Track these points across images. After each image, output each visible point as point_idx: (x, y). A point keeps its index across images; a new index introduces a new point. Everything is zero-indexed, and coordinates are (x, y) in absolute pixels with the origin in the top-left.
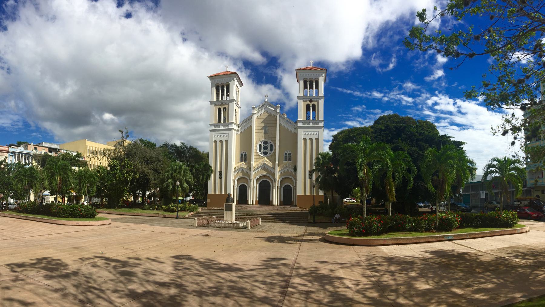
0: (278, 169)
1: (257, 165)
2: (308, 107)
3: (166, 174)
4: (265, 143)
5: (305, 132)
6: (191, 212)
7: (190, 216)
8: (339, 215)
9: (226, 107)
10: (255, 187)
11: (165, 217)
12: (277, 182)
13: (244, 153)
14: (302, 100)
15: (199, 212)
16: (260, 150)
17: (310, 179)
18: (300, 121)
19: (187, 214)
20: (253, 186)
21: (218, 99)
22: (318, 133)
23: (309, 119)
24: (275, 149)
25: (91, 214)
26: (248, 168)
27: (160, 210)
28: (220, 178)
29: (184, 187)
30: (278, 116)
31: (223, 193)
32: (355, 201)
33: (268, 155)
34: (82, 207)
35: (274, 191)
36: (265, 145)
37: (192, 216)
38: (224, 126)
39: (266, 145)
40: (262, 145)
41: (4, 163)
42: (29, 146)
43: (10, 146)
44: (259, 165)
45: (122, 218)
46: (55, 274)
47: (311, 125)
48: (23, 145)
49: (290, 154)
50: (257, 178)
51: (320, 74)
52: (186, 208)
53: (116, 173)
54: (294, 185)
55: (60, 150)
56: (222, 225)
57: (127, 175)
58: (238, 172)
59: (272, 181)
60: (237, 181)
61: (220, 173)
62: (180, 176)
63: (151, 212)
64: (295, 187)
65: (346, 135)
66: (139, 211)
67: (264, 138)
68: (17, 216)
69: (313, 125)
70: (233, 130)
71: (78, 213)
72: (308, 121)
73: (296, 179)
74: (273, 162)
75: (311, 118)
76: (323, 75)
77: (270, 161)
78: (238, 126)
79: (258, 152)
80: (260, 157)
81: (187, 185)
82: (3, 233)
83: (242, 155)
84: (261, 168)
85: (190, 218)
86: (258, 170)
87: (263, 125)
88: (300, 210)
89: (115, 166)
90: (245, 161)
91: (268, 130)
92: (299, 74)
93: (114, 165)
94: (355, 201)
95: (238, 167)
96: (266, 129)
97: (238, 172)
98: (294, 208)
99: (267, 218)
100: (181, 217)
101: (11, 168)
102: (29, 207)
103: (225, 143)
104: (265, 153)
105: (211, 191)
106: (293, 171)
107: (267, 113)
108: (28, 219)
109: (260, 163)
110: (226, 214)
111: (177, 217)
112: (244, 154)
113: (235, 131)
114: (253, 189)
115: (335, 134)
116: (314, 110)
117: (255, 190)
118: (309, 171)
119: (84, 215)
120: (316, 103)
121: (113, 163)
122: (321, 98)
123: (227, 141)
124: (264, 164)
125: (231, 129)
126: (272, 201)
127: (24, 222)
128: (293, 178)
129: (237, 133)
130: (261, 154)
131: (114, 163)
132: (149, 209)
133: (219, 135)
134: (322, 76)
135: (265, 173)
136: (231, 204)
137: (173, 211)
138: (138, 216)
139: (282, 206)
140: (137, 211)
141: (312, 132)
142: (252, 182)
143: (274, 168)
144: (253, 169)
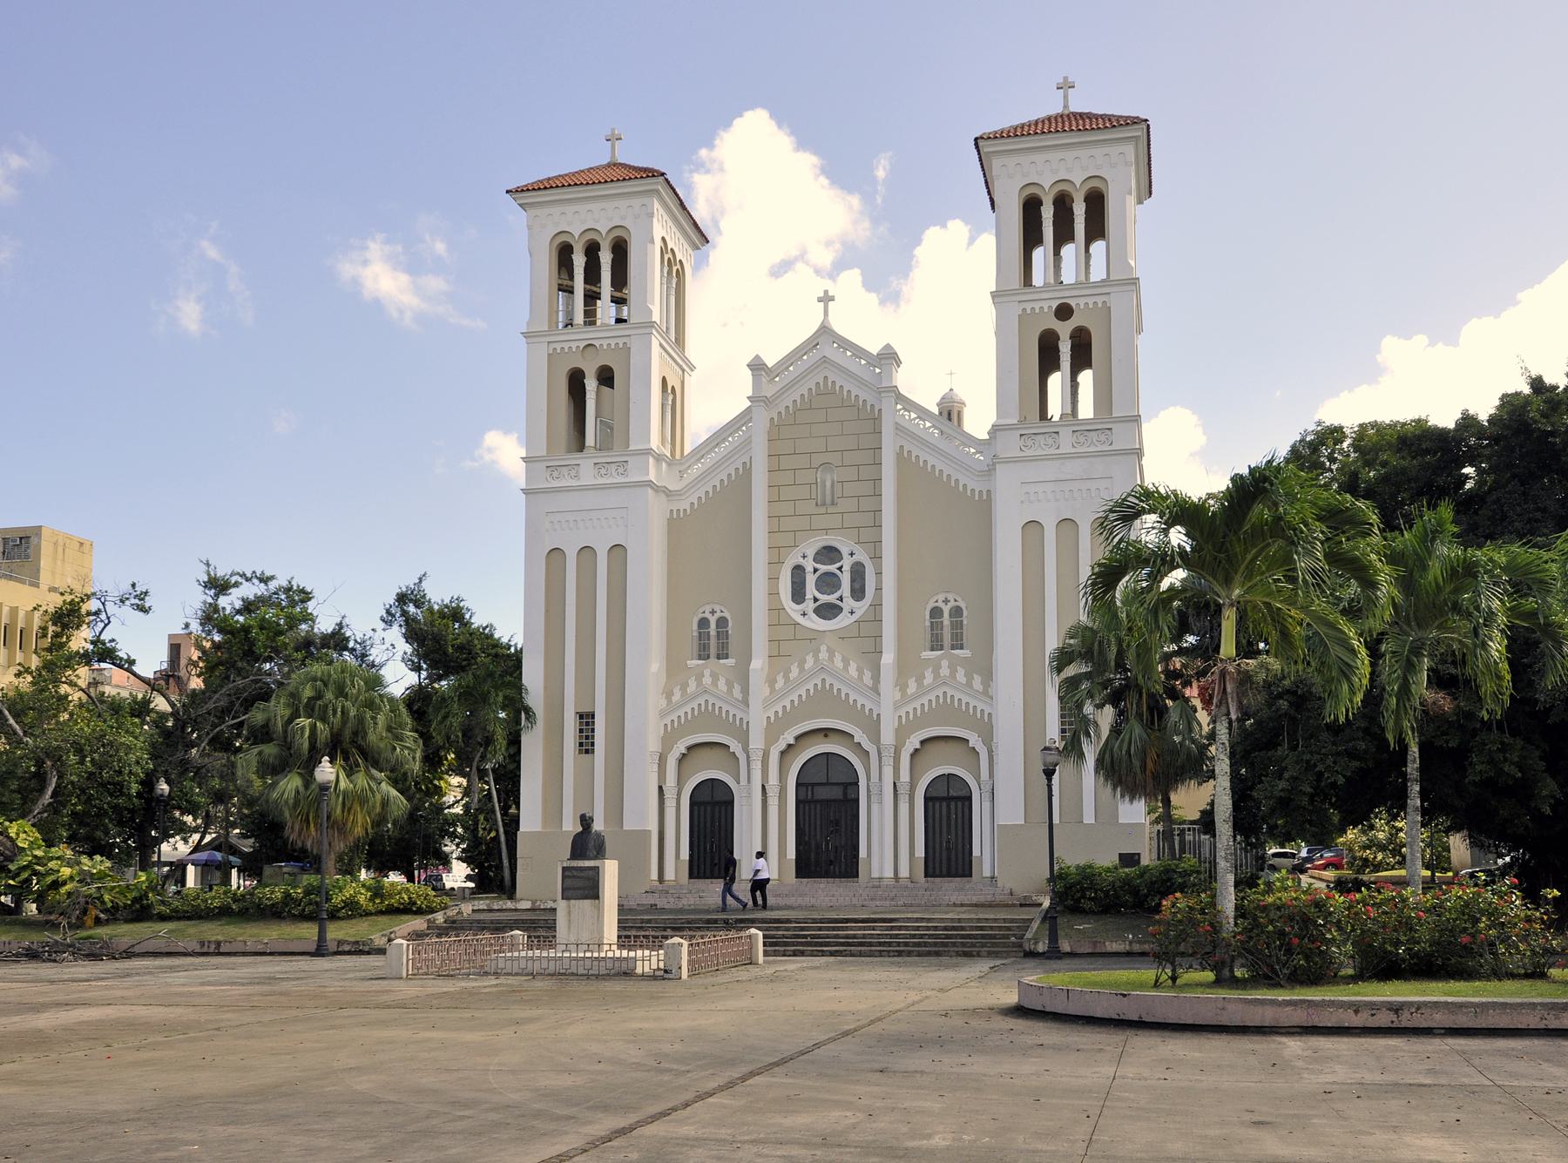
36: (823, 568)
39: (832, 568)
40: (809, 569)
91: (838, 487)
92: (984, 150)
111: (320, 951)
112: (946, 610)
128: (974, 740)
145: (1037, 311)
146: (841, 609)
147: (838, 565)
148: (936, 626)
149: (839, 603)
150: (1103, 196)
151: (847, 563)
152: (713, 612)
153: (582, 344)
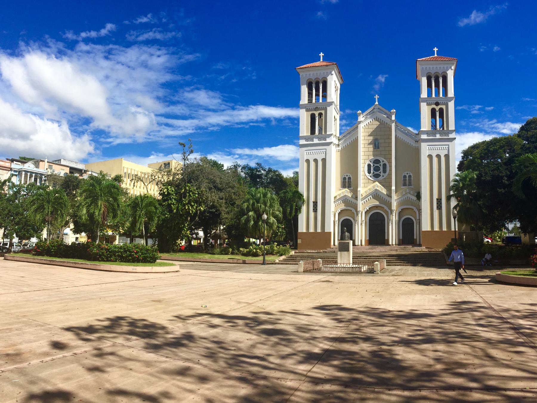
0: (394, 197)
1: (366, 192)
2: (433, 112)
3: (245, 205)
4: (376, 161)
5: (430, 147)
6: (281, 255)
7: (281, 261)
8: (490, 255)
9: (323, 112)
10: (364, 222)
11: (244, 262)
12: (394, 214)
13: (347, 176)
14: (425, 104)
15: (291, 256)
16: (369, 172)
17: (439, 209)
19: (278, 259)
20: (362, 221)
21: (310, 100)
22: (448, 148)
23: (436, 129)
24: (391, 170)
25: (151, 257)
26: (354, 197)
27: (237, 254)
28: (315, 210)
29: (270, 223)
30: (393, 125)
31: (319, 230)
32: (490, 241)
33: (381, 178)
34: (137, 248)
35: (390, 227)
36: (376, 165)
37: (285, 261)
38: (320, 139)
39: (378, 165)
40: (372, 165)
41: (7, 184)
42: (41, 163)
43: (12, 161)
44: (369, 192)
45: (186, 265)
46: (158, 341)
47: (438, 136)
48: (31, 161)
49: (349, 178)
50: (366, 210)
51: (449, 66)
52: (274, 250)
53: (171, 204)
54: (418, 218)
55: (86, 171)
56: (338, 270)
57: (189, 207)
58: (340, 202)
59: (387, 213)
60: (339, 214)
61: (315, 204)
62: (265, 207)
63: (226, 257)
64: (419, 221)
65: (485, 150)
66: (207, 257)
67: (374, 155)
68: (34, 259)
69: (441, 137)
70: (332, 144)
71: (133, 255)
72: (434, 131)
73: (420, 210)
74: (389, 188)
75: (438, 127)
76: (333, 72)
77: (383, 186)
78: (339, 140)
80: (370, 181)
81: (274, 219)
82: (27, 282)
83: (345, 178)
84: (371, 196)
85: (282, 264)
86: (367, 199)
87: (371, 138)
88: (427, 250)
89: (169, 194)
90: (349, 187)
93: (168, 192)
94: (490, 241)
95: (339, 195)
96: (377, 143)
97: (340, 202)
98: (419, 248)
99: (390, 261)
100: (270, 262)
101: (19, 192)
102: (52, 247)
103: (321, 162)
104: (376, 176)
105: (302, 228)
106: (415, 198)
107: (378, 121)
108: (54, 263)
109: (369, 189)
110: (341, 255)
111: (264, 263)
112: (347, 178)
113: (335, 146)
114: (361, 224)
115: (465, 149)
116: (441, 116)
117: (364, 225)
118: (437, 199)
119: (141, 258)
120: (444, 107)
121: (165, 190)
122: (450, 99)
123: (324, 160)
125: (329, 144)
126: (388, 240)
127: (50, 268)
128: (415, 208)
129: (338, 148)
130: (371, 177)
131: (168, 189)
132: (221, 253)
133: (313, 151)
135: (377, 203)
136: (347, 241)
137: (256, 255)
138: (206, 262)
139: (401, 246)
140: (203, 256)
141: (440, 147)
142: (360, 215)
143: (390, 196)
144: (360, 197)
146: (380, 175)
147: (380, 164)
151: (382, 163)
153: (315, 107)
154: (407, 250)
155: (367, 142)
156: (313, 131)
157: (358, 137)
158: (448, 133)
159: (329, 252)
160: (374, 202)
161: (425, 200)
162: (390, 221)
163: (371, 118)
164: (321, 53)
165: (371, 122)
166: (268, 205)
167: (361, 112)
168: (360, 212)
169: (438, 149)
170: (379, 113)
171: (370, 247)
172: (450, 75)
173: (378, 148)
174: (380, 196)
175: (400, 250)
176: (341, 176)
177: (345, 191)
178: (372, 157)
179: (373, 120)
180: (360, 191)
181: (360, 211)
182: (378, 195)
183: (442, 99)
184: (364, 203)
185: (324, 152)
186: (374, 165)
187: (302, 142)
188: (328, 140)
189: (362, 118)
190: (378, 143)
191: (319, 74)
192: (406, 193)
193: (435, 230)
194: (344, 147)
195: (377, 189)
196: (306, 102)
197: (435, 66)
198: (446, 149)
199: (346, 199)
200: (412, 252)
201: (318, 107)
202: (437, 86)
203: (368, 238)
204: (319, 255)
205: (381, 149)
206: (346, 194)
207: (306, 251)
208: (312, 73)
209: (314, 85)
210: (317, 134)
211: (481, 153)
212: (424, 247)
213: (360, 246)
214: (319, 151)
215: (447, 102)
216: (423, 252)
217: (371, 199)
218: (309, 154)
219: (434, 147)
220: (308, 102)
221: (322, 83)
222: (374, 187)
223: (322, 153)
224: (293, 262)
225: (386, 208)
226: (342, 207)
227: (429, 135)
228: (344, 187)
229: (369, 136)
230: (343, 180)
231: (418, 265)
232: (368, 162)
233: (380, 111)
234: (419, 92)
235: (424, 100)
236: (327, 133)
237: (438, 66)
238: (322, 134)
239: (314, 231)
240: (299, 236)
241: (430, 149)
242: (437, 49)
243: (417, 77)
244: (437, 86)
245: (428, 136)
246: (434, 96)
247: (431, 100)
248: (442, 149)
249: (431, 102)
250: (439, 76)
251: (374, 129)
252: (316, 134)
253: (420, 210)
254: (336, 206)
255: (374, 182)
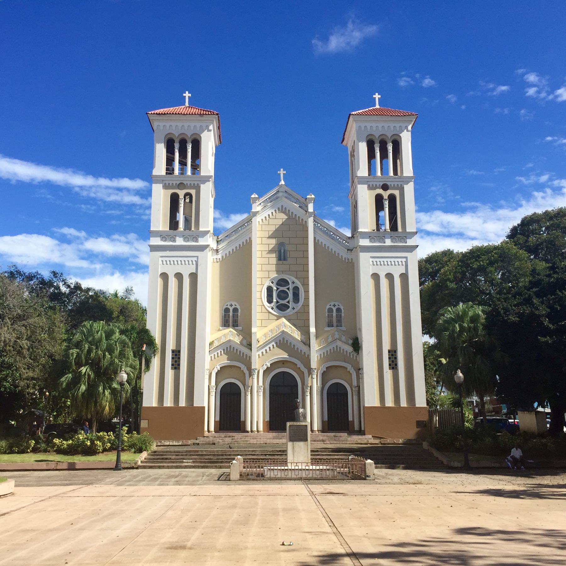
1: (265, 335)
2: (379, 200)
4: (282, 282)
5: (374, 260)
8: (519, 450)
9: (193, 192)
13: (231, 305)
14: (366, 186)
16: (270, 301)
17: (175, 368)
18: (365, 235)
21: (170, 170)
24: (307, 298)
26: (245, 342)
28: (176, 366)
30: (311, 222)
31: (183, 403)
36: (281, 288)
38: (186, 239)
39: (284, 289)
44: (271, 336)
49: (235, 310)
50: (265, 367)
51: (403, 125)
54: (355, 383)
61: (176, 354)
64: (357, 389)
67: (278, 271)
69: (393, 244)
73: (359, 370)
74: (304, 329)
76: (211, 127)
78: (217, 242)
79: (266, 304)
80: (271, 317)
83: (227, 310)
84: (273, 343)
86: (267, 348)
87: (273, 241)
90: (235, 325)
95: (218, 339)
96: (282, 251)
97: (219, 352)
98: (360, 437)
100: (126, 466)
103: (188, 280)
104: (282, 308)
106: (350, 349)
107: (285, 213)
109: (271, 331)
110: (293, 448)
111: (117, 467)
118: (389, 351)
120: (397, 193)
122: (407, 180)
123: (194, 277)
124: (283, 332)
125: (203, 248)
126: (244, 423)
128: (349, 367)
129: (215, 257)
130: (272, 308)
134: (408, 131)
135: (284, 355)
141: (392, 260)
142: (255, 377)
144: (254, 345)
145: (171, 185)
147: (287, 287)
148: (330, 316)
149: (287, 304)
150: (199, 141)
151: (291, 286)
152: (330, 305)
153: (178, 182)
154: (343, 441)
155: (266, 248)
156: (174, 224)
157: (250, 238)
158: (406, 237)
159: (203, 444)
160: (280, 354)
161: (369, 353)
162: (307, 388)
163: (272, 207)
164: (187, 92)
165: (272, 215)
166: (117, 352)
167: (257, 196)
168: (256, 371)
169: (388, 265)
170: (286, 200)
171: (274, 434)
172: (406, 139)
173: (284, 260)
174: (290, 343)
175: (329, 441)
176: (221, 306)
177: (228, 334)
178: (274, 275)
179: (277, 211)
180: (255, 333)
181: (256, 369)
182: (287, 341)
183: (394, 180)
184: (263, 355)
185: (194, 263)
186: (278, 289)
187: (156, 241)
188: (202, 242)
189: (258, 206)
190: (284, 251)
191: (186, 128)
192: (334, 340)
193: (386, 406)
194: (226, 254)
195: (285, 330)
196: (163, 172)
197: (380, 125)
198: (402, 265)
199: (230, 346)
200: (352, 444)
201: (185, 183)
202: (384, 155)
203: (268, 419)
204: (185, 449)
205: (290, 261)
206: (231, 338)
207: (160, 442)
208: (174, 124)
209: (177, 146)
210: (182, 230)
211: (455, 272)
212: (370, 436)
213: (256, 432)
214: (185, 259)
215: (198, 184)
216: (370, 444)
217: (273, 347)
218: (167, 264)
219: (382, 260)
220: (167, 173)
221: (192, 143)
222: (278, 327)
223: (191, 263)
224: (169, 463)
225: (299, 364)
226: (224, 361)
227: (373, 240)
228: (225, 326)
229: (269, 237)
230: (224, 313)
231: (398, 468)
232: (267, 283)
233: (289, 196)
234: (353, 166)
235: (363, 181)
236: (201, 229)
237: (374, 125)
238: (190, 229)
239: (173, 406)
240: (143, 414)
241: (375, 263)
242: (380, 96)
243: (343, 141)
244: (384, 155)
245: (371, 241)
246: (379, 174)
247: (375, 180)
248: (395, 265)
249: (374, 184)
250: (388, 141)
251: (277, 226)
252: (179, 230)
253: (360, 369)
254: (211, 360)
255: (278, 318)
